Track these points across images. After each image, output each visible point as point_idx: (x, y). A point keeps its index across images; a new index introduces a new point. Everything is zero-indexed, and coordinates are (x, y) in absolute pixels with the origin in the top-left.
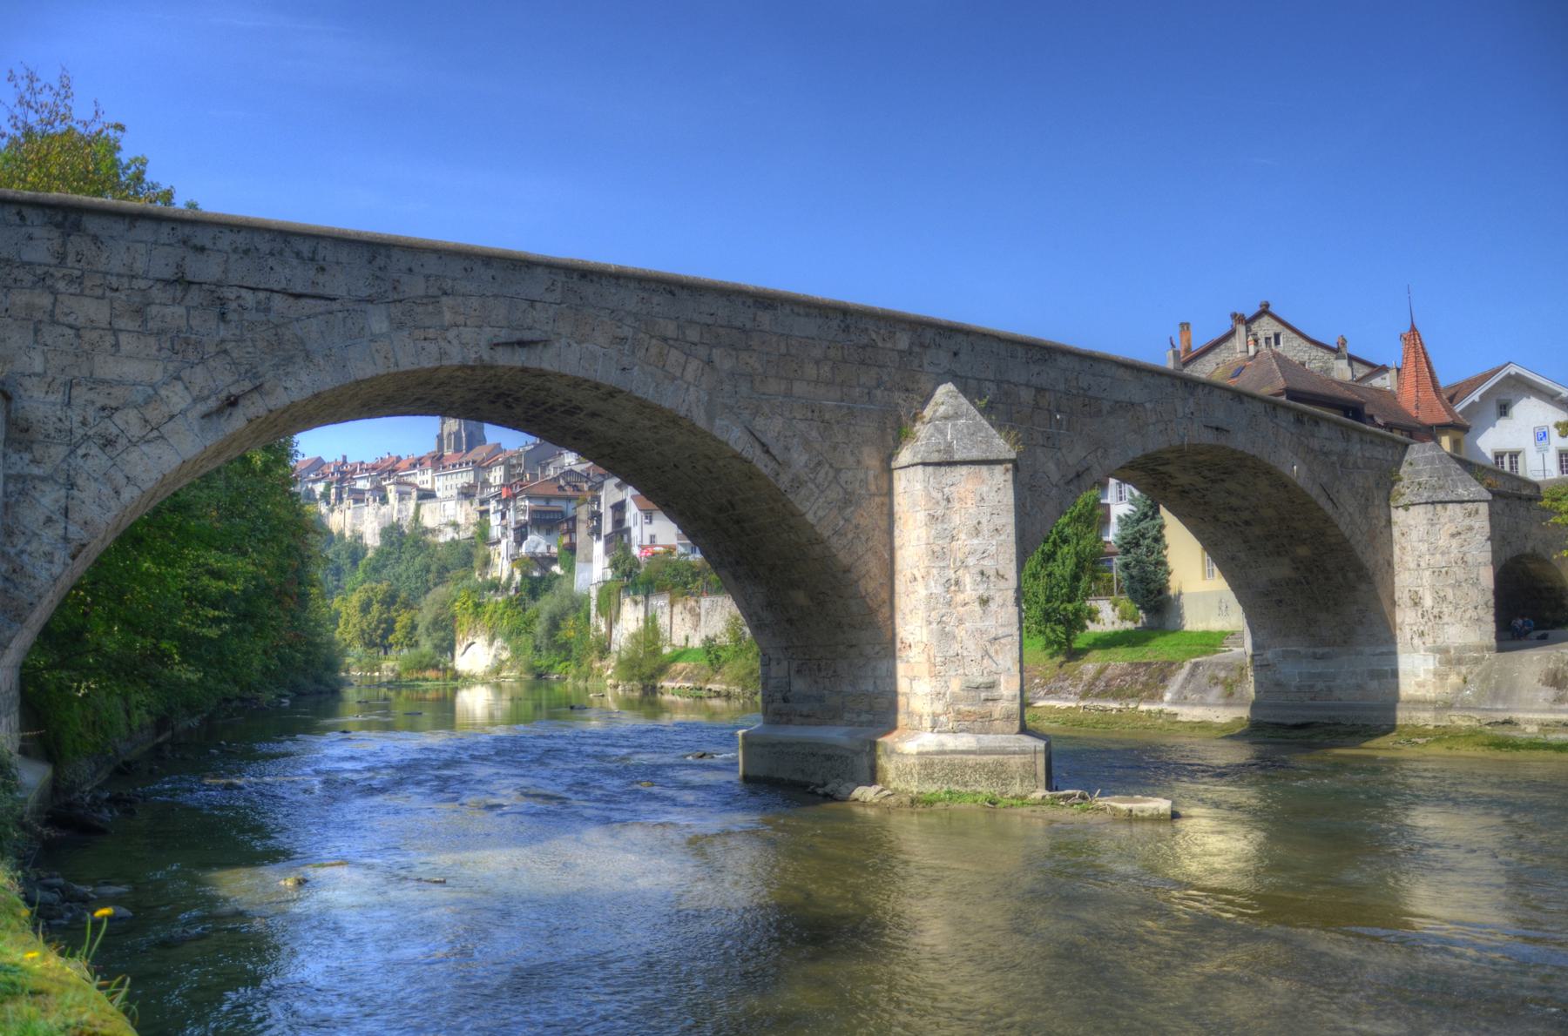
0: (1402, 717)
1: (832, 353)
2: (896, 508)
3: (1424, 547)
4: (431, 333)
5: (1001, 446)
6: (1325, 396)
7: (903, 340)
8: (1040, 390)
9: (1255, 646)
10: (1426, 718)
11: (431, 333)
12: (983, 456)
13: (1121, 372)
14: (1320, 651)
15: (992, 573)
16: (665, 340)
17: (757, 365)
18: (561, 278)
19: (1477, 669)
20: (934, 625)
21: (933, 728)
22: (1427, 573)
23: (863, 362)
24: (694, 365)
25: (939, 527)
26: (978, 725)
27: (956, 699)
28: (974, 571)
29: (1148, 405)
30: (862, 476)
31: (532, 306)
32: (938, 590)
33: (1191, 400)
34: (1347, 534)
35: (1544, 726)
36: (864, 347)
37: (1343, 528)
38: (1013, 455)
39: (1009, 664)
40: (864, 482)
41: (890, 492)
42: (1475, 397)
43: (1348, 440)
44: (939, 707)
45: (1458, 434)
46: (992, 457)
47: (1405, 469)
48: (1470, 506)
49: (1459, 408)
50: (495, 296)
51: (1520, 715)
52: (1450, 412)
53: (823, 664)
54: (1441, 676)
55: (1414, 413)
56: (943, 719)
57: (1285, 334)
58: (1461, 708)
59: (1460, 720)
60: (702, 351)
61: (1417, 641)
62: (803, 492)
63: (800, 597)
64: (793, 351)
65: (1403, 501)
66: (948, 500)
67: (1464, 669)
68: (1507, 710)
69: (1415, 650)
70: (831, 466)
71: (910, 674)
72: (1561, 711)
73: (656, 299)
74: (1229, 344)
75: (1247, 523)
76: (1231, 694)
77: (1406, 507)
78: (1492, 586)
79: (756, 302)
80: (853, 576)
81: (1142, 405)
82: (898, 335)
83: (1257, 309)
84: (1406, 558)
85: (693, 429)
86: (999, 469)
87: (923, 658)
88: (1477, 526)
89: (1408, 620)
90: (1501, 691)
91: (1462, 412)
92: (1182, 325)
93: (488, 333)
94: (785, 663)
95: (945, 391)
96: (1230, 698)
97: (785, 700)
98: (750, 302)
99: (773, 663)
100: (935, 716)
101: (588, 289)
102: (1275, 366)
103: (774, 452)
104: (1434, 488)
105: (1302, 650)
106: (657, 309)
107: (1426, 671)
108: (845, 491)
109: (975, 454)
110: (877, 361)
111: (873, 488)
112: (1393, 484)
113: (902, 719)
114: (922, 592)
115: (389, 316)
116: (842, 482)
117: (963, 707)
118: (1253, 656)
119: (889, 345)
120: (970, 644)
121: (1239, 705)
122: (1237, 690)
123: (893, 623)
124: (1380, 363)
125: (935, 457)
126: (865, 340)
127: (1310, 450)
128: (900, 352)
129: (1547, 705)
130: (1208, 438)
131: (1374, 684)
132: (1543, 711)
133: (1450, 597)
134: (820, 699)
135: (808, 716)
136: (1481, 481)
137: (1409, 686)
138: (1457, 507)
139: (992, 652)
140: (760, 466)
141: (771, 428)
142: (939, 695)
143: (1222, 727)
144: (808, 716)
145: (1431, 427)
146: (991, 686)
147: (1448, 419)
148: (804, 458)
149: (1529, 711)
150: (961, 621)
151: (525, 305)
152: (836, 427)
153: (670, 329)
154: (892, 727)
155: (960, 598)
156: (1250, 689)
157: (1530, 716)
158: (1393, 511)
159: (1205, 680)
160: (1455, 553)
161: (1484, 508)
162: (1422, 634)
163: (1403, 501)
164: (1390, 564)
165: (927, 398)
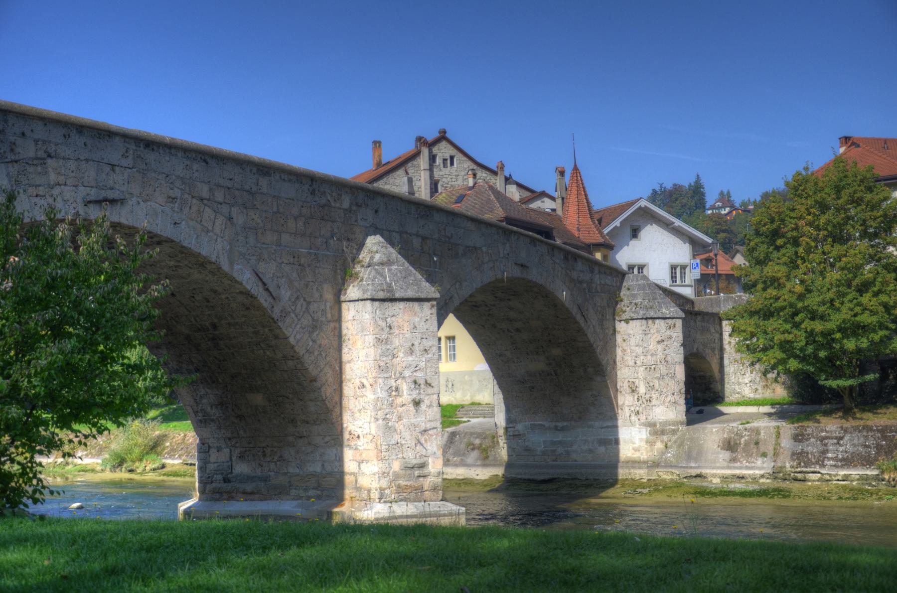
0: (622, 473)
1: (304, 211)
2: (344, 332)
3: (639, 350)
4: (41, 191)
5: (429, 290)
6: (529, 223)
7: (346, 202)
8: (424, 238)
9: (509, 420)
10: (641, 474)
11: (41, 191)
12: (417, 295)
13: (470, 225)
14: (560, 424)
15: (422, 382)
16: (202, 200)
17: (259, 221)
18: (133, 147)
19: (674, 438)
20: (380, 422)
21: (380, 499)
22: (642, 369)
23: (323, 219)
24: (220, 220)
25: (384, 347)
26: (413, 495)
27: (397, 476)
28: (409, 380)
29: (484, 249)
30: (323, 307)
31: (113, 170)
32: (383, 395)
34: (592, 340)
35: (724, 478)
36: (323, 206)
37: (589, 336)
38: (438, 295)
39: (435, 449)
40: (324, 311)
41: (339, 319)
42: (617, 223)
43: (592, 272)
44: (384, 483)
45: (606, 251)
46: (423, 296)
47: (624, 292)
48: (670, 321)
49: (606, 231)
50: (87, 160)
51: (708, 471)
52: (601, 233)
53: (268, 451)
54: (651, 443)
55: (576, 234)
56: (387, 492)
58: (666, 467)
59: (665, 475)
60: (225, 209)
61: (633, 418)
62: (288, 320)
63: (258, 399)
64: (281, 210)
65: (624, 317)
66: (390, 328)
67: (665, 438)
68: (698, 467)
69: (633, 425)
70: (305, 300)
71: (358, 458)
72: (735, 468)
73: (196, 166)
74: (415, 163)
75: (518, 330)
76: (487, 457)
77: (627, 321)
78: (684, 379)
79: (258, 170)
80: (318, 384)
82: (343, 196)
83: (436, 135)
84: (626, 358)
85: (217, 271)
86: (427, 305)
87: (371, 446)
88: (674, 335)
89: (627, 403)
90: (693, 453)
91: (607, 234)
92: (375, 142)
93: (83, 191)
94: (226, 451)
95: (373, 242)
96: (486, 459)
97: (226, 480)
98: (255, 170)
99: (212, 451)
100: (382, 490)
101: (151, 156)
102: (492, 197)
103: (271, 289)
104: (647, 308)
105: (547, 424)
106: (196, 174)
107: (641, 440)
108: (313, 320)
109: (410, 294)
110: (333, 214)
111: (329, 316)
112: (617, 303)
113: (348, 492)
114: (370, 396)
115: (8, 174)
116: (311, 311)
117: (402, 483)
118: (506, 429)
119: (338, 205)
120: (407, 434)
121: (494, 465)
122: (491, 454)
123: (342, 419)
124: (538, 189)
125: (381, 295)
126: (323, 201)
128: (345, 210)
129: (725, 464)
130: (517, 272)
131: (602, 449)
132: (723, 468)
133: (657, 386)
134: (265, 479)
135: (252, 493)
136: (679, 306)
137: (626, 451)
138: (662, 321)
139: (423, 441)
140: (262, 301)
141: (269, 269)
142: (384, 474)
143: (484, 483)
144: (252, 493)
145: (589, 246)
146: (422, 466)
147: (601, 240)
148: (288, 294)
149: (713, 468)
150: (400, 418)
151: (107, 169)
152: (307, 269)
153: (205, 192)
154: (340, 500)
155: (399, 400)
156: (503, 452)
157: (714, 471)
158: (617, 323)
159: (463, 446)
160: (660, 356)
161: (679, 323)
162: (638, 413)
163: (624, 317)
164: (615, 362)
165: (361, 245)
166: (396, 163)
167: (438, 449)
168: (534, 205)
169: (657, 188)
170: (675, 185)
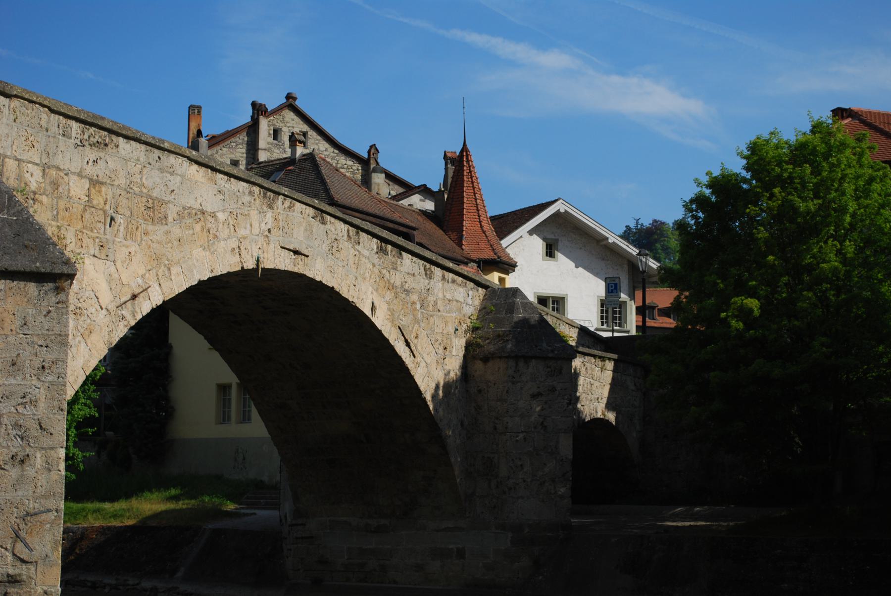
8: (95, 183)
29: (221, 216)
33: (270, 214)
57: (312, 134)
81: (213, 215)
92: (192, 108)
127: (391, 287)
166: (368, 218)
167: (54, 549)
168: (405, 202)
169: (632, 225)
170: (655, 221)
